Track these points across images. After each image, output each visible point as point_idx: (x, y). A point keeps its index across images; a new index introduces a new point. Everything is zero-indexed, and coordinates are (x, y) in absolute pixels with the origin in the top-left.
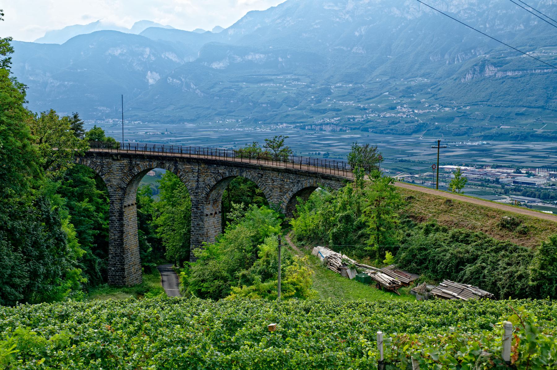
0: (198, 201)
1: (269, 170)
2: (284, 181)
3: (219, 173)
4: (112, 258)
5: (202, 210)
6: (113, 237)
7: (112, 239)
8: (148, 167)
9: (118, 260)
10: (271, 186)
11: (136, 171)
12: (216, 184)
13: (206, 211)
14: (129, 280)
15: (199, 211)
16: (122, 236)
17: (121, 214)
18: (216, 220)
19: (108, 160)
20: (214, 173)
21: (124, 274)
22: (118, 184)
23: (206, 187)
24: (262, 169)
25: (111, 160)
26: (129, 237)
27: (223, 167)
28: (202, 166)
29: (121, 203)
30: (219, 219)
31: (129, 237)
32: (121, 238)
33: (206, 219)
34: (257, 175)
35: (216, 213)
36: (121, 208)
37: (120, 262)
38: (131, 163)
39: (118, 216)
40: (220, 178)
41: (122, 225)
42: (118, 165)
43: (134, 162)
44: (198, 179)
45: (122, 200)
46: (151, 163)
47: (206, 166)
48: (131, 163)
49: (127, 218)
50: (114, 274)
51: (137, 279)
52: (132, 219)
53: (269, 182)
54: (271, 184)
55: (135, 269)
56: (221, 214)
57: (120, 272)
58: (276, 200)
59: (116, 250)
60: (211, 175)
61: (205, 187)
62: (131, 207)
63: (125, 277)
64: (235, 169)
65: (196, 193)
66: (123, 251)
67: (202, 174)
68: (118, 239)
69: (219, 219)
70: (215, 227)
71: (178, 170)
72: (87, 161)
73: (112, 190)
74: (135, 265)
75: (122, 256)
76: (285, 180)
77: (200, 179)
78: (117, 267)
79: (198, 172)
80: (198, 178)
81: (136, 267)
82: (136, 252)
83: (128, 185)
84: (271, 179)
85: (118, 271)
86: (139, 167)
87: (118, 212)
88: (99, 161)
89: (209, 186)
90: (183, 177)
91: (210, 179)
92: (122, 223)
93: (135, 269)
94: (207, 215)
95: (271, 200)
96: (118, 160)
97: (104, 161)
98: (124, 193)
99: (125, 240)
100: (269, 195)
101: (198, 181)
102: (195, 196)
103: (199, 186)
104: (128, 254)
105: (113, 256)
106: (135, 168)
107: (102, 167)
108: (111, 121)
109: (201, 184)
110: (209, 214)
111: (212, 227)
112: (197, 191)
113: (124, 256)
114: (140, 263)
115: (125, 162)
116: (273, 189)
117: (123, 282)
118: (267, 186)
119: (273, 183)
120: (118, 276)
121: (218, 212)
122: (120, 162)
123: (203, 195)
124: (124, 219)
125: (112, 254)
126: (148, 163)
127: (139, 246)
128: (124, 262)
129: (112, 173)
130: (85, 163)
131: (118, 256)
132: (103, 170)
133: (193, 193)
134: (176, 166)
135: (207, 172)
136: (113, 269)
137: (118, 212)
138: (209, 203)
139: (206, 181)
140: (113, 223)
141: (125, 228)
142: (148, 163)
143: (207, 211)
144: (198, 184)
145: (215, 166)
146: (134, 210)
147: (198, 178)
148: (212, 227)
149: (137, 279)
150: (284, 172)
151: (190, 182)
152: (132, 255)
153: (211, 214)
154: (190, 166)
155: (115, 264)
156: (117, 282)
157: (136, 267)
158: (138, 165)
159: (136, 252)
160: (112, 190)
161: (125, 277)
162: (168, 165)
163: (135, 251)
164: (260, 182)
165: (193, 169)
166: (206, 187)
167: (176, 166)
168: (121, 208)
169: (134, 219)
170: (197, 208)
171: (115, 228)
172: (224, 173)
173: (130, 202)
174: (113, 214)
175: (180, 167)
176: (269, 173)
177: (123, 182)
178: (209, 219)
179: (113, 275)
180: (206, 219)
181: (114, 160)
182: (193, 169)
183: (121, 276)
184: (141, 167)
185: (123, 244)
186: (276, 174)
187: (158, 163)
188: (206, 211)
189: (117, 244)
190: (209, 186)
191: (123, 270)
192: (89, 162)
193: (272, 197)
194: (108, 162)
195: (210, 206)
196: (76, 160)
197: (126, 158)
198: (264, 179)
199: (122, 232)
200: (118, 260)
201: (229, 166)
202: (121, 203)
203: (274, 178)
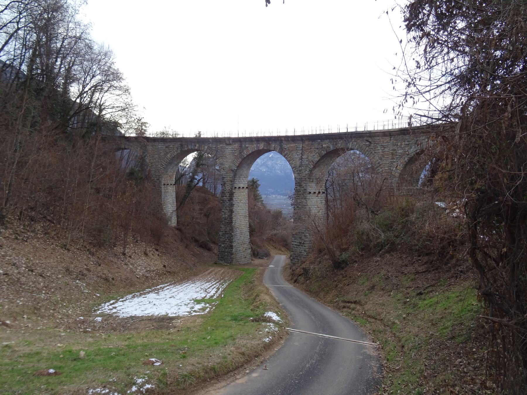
0: (302, 178)
1: (378, 136)
2: (397, 145)
3: (323, 147)
4: (222, 235)
5: (305, 188)
6: (224, 216)
7: (223, 218)
8: (256, 149)
9: (228, 238)
10: (380, 153)
11: (245, 153)
12: (319, 160)
13: (309, 189)
14: (237, 257)
15: (303, 189)
16: (231, 215)
17: (232, 194)
18: (319, 200)
19: (222, 145)
20: (318, 148)
21: (232, 251)
22: (230, 167)
23: (310, 164)
24: (370, 137)
25: (224, 145)
26: (239, 217)
27: (327, 141)
28: (307, 143)
29: (231, 185)
30: (322, 200)
31: (239, 217)
32: (231, 217)
33: (308, 196)
34: (364, 143)
35: (319, 193)
36: (232, 188)
37: (229, 240)
38: (241, 146)
39: (229, 196)
40: (324, 153)
41: (232, 205)
42: (230, 150)
43: (243, 146)
44: (301, 157)
45: (232, 181)
46: (258, 145)
47: (310, 142)
48: (241, 146)
49: (237, 199)
50: (223, 250)
51: (246, 257)
52: (242, 201)
53: (379, 150)
54: (381, 151)
55: (243, 248)
56: (324, 195)
57: (229, 248)
58: (387, 168)
59: (226, 228)
60: (315, 151)
61: (309, 164)
62: (241, 190)
63: (233, 254)
64: (340, 141)
65: (300, 171)
66: (232, 230)
67: (306, 151)
68: (228, 218)
69: (322, 200)
70: (318, 207)
71: (283, 150)
72: (204, 147)
73: (224, 172)
74: (244, 244)
75: (231, 234)
76: (399, 144)
77: (304, 157)
78: (226, 244)
79: (302, 149)
80: (302, 155)
81: (245, 246)
82: (246, 232)
83: (238, 167)
84: (381, 146)
85: (227, 248)
86: (248, 150)
87: (228, 192)
88: (214, 147)
89: (313, 162)
90: (288, 156)
91: (314, 155)
92: (232, 203)
93: (243, 248)
94: (310, 193)
95: (381, 170)
96: (230, 144)
97: (219, 147)
98: (235, 175)
99: (234, 219)
100: (379, 163)
101: (301, 159)
102: (298, 173)
103: (303, 163)
104: (237, 233)
105: (224, 234)
106: (245, 151)
107: (217, 152)
108: (274, 196)
109: (305, 162)
110: (312, 192)
111: (315, 206)
112: (300, 169)
113: (233, 234)
114: (250, 243)
115: (236, 146)
116: (383, 156)
117: (231, 258)
118: (376, 154)
119: (384, 149)
120: (227, 252)
121: (321, 192)
122: (232, 146)
123: (307, 172)
124: (234, 200)
125: (222, 231)
126: (255, 145)
127: (249, 227)
128: (232, 240)
129: (225, 157)
130: (202, 148)
131: (228, 234)
132: (217, 154)
133: (297, 171)
134: (281, 146)
135: (311, 148)
136: (223, 245)
137: (228, 192)
138: (312, 181)
139: (310, 158)
140: (224, 203)
141: (235, 209)
142: (255, 145)
143: (310, 189)
144: (301, 162)
145: (319, 141)
146: (245, 193)
147: (302, 155)
148: (315, 206)
149: (246, 257)
150: (398, 135)
151: (294, 161)
152: (241, 234)
153: (315, 193)
154: (294, 145)
155: (225, 241)
156: (226, 258)
157: (245, 246)
158: (247, 147)
159: (246, 232)
160: (224, 172)
161: (233, 254)
162: (274, 145)
163: (244, 231)
164: (367, 150)
165: (297, 147)
166: (310, 164)
167: (281, 146)
168: (232, 188)
169: (244, 201)
170: (300, 186)
171: (226, 208)
172: (328, 147)
173: (241, 185)
174: (225, 194)
175: (285, 146)
176: (379, 139)
177: (234, 164)
178: (313, 197)
179: (223, 252)
180: (308, 196)
181: (227, 144)
182: (297, 147)
183: (229, 252)
184: (249, 149)
185: (232, 223)
186: (387, 139)
187: (264, 144)
188: (309, 189)
189: (227, 222)
190: (313, 162)
191: (231, 247)
192: (206, 147)
193: (381, 166)
194: (222, 147)
195: (313, 185)
196: (196, 146)
197: (237, 142)
198: (372, 147)
199: (231, 211)
200: (228, 238)
201: (333, 139)
202: (231, 185)
203: (384, 144)
